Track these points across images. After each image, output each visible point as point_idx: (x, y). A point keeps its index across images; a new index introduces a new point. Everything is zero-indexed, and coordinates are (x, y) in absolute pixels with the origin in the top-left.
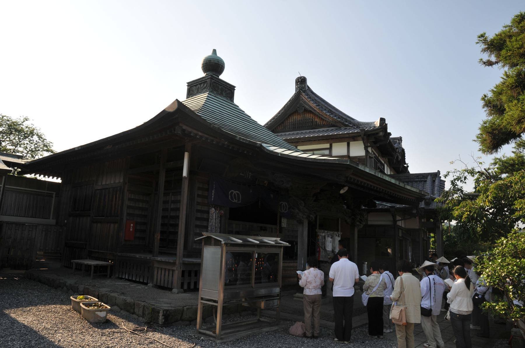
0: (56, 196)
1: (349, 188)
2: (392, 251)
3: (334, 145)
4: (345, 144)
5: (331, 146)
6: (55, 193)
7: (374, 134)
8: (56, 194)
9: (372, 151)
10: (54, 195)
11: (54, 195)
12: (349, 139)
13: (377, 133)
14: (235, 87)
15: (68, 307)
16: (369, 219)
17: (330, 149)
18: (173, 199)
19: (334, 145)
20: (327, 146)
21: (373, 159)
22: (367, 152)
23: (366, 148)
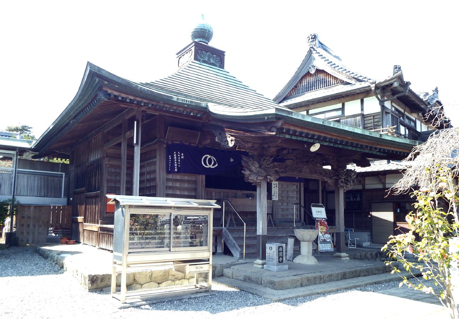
0: (65, 177)
1: (321, 146)
2: (72, 199)
3: (346, 104)
4: (359, 101)
5: (343, 105)
6: (64, 174)
7: (387, 86)
8: (65, 175)
9: (392, 106)
10: (64, 176)
11: (64, 176)
12: (362, 94)
13: (392, 84)
14: (224, 52)
15: (336, 285)
16: (366, 183)
17: (343, 109)
18: (148, 170)
19: (347, 104)
20: (340, 106)
21: (390, 115)
22: (383, 107)
23: (382, 103)
